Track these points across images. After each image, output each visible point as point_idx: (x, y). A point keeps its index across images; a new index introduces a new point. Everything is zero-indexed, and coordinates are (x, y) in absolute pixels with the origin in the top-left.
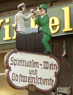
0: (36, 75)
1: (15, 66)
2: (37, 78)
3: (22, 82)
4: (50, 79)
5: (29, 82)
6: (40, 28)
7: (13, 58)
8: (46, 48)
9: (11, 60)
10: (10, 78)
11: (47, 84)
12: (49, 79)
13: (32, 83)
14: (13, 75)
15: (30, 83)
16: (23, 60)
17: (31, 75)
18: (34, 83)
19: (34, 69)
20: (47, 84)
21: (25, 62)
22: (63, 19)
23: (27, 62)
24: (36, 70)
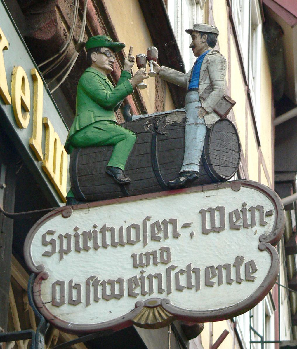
0: (164, 263)
1: (61, 258)
2: (173, 273)
3: (101, 302)
4: (239, 260)
5: (131, 295)
6: (170, 181)
7: (51, 233)
8: (217, 79)
9: (45, 244)
10: (52, 127)
11: (224, 280)
12: (232, 262)
13: (147, 297)
14: (58, 288)
15: (140, 298)
16: (98, 229)
17: (144, 251)
18: (160, 291)
19: (153, 246)
20: (224, 280)
21: (108, 235)
22: (291, 228)
23: (121, 229)
24: (167, 250)
